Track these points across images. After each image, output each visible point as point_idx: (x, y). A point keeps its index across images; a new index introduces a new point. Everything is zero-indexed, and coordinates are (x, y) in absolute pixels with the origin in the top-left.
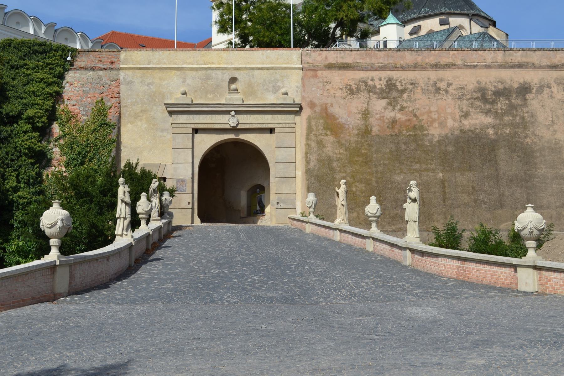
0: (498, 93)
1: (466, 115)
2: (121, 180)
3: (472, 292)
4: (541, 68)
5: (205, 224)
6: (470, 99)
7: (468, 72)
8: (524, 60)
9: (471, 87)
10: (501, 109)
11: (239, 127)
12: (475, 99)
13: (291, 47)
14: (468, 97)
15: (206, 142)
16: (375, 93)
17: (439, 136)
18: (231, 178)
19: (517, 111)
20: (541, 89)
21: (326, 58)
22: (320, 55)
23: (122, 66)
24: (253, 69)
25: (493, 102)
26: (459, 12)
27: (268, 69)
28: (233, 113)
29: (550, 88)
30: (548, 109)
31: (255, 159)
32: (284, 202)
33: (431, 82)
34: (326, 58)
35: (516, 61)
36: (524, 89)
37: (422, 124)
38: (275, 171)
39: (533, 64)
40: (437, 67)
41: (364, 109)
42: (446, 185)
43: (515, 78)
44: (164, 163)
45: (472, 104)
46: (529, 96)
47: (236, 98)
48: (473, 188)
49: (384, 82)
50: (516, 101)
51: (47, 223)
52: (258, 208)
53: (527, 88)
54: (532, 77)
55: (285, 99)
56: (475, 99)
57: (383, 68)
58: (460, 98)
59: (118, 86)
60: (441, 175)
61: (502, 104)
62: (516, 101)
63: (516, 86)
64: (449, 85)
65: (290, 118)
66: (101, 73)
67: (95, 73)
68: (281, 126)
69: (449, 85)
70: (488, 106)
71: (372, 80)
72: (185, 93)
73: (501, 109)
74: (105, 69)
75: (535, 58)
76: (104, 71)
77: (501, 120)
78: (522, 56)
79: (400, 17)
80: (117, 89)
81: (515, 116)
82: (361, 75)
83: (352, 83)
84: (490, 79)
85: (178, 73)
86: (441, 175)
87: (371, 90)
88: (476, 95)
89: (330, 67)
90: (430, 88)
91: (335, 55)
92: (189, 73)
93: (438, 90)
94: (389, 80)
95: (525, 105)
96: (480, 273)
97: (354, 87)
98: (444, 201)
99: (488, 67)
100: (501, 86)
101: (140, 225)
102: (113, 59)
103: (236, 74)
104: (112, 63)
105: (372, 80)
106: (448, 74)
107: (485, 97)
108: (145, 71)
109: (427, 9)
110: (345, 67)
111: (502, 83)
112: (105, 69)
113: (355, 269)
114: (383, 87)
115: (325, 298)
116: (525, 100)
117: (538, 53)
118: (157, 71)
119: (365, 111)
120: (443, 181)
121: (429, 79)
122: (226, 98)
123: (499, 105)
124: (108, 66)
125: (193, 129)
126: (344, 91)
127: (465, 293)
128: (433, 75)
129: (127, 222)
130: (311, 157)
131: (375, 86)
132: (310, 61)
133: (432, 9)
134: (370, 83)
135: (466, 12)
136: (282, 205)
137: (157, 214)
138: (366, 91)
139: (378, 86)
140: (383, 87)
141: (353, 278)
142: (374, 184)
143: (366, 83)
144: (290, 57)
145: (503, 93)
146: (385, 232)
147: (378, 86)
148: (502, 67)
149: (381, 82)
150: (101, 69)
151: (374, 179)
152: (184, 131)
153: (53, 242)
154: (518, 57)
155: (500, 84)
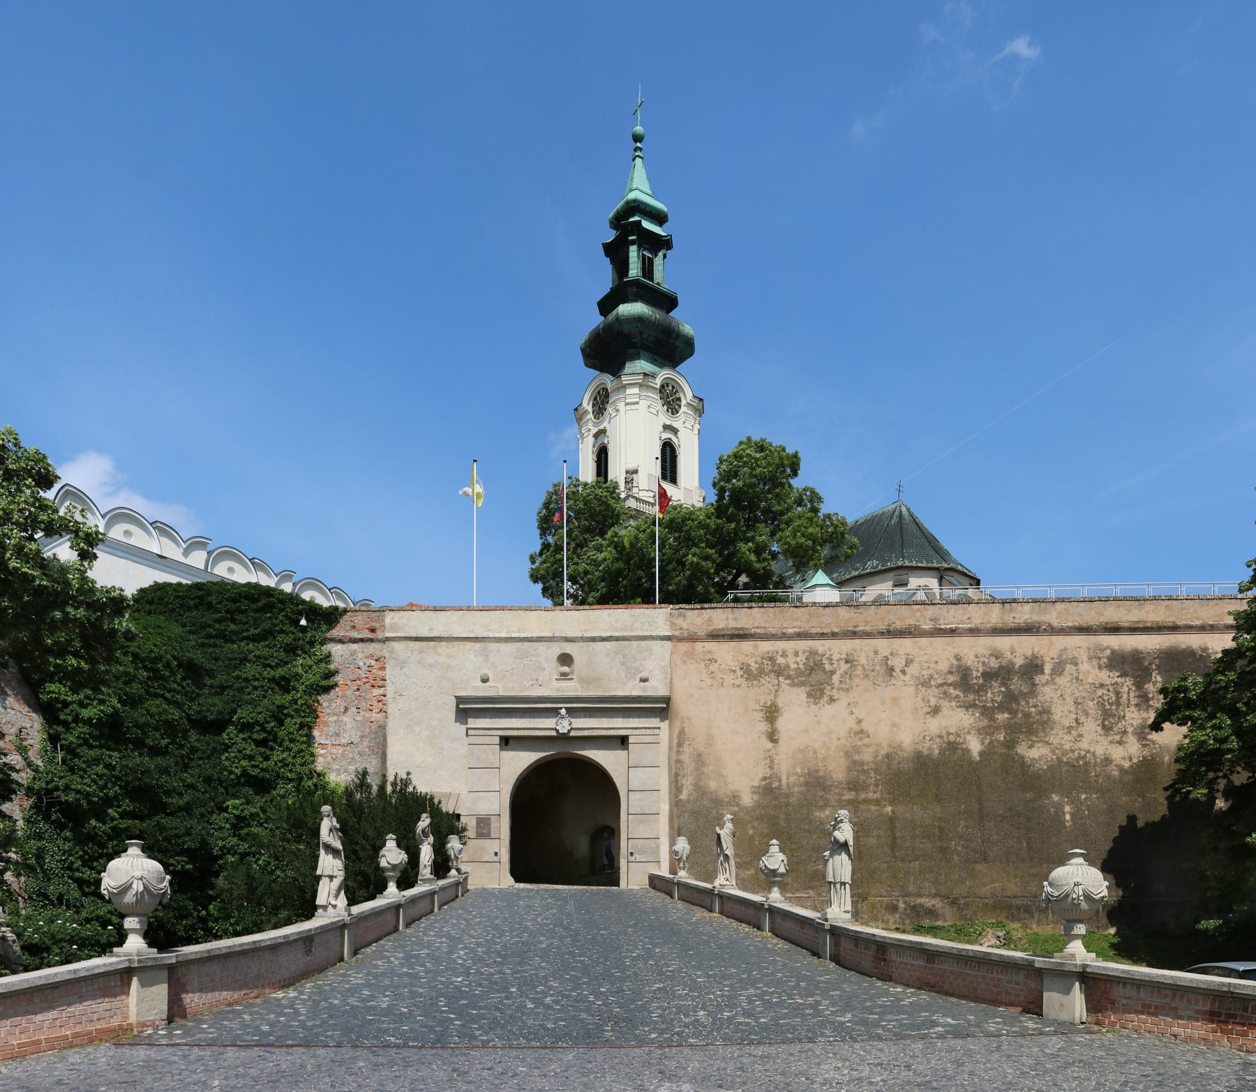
0: (988, 675)
1: (935, 711)
2: (326, 809)
3: (949, 1020)
4: (1062, 631)
5: (522, 885)
6: (942, 685)
7: (939, 642)
8: (1036, 618)
9: (944, 666)
10: (993, 701)
11: (573, 734)
12: (950, 685)
13: (654, 602)
14: (940, 681)
15: (524, 759)
16: (788, 677)
17: (890, 746)
18: (563, 816)
19: (1018, 704)
20: (1058, 670)
21: (710, 619)
22: (699, 616)
23: (388, 635)
24: (593, 639)
25: (981, 690)
26: (924, 565)
27: (617, 639)
28: (563, 712)
29: (1076, 664)
30: (1070, 700)
31: (602, 788)
32: (642, 852)
33: (879, 657)
34: (710, 619)
35: (1022, 621)
36: (1033, 667)
37: (849, 916)
38: (630, 804)
39: (1050, 625)
40: (890, 633)
41: (769, 703)
42: (898, 824)
43: (1018, 649)
44: (457, 791)
45: (945, 693)
46: (1039, 679)
47: (571, 689)
48: (941, 829)
49: (802, 658)
50: (1017, 685)
51: (113, 884)
52: (606, 862)
53: (1037, 666)
54: (1047, 648)
55: (644, 689)
56: (950, 685)
57: (801, 636)
58: (925, 684)
59: (383, 668)
60: (889, 809)
61: (994, 693)
62: (1017, 685)
63: (1019, 662)
64: (909, 662)
65: (653, 722)
66: (355, 646)
67: (345, 646)
68: (638, 732)
69: (909, 662)
70: (971, 697)
71: (784, 655)
72: (485, 680)
73: (993, 701)
74: (362, 640)
75: (1053, 616)
76: (361, 645)
77: (992, 719)
78: (1032, 612)
79: (835, 575)
80: (381, 673)
81: (1013, 712)
82: (766, 646)
83: (751, 662)
84: (974, 651)
85: (478, 645)
86: (889, 809)
87: (779, 672)
88: (951, 679)
89: (715, 636)
90: (878, 668)
91: (724, 616)
92: (493, 646)
93: (891, 670)
94: (813, 653)
95: (1033, 692)
96: (965, 980)
97: (754, 667)
98: (892, 849)
99: (974, 632)
100: (994, 663)
101: (385, 888)
102: (374, 624)
103: (568, 648)
104: (373, 630)
105: (784, 655)
106: (905, 645)
107: (964, 681)
108: (424, 644)
109: (875, 563)
110: (740, 635)
111: (997, 658)
112: (362, 640)
113: (733, 967)
114: (801, 666)
115: (662, 1032)
116: (1034, 685)
117: (1059, 606)
118: (444, 644)
119: (770, 707)
120: (892, 820)
121: (876, 653)
122: (552, 687)
123: (989, 695)
124: (366, 634)
125: (501, 737)
126: (739, 673)
127: (935, 1024)
128: (883, 645)
129: (337, 882)
130: (684, 781)
131: (787, 666)
132: (685, 626)
133: (884, 561)
134: (780, 660)
135: (935, 565)
136: (638, 857)
137: (428, 870)
138: (772, 675)
139: (793, 666)
140: (801, 666)
141: (726, 986)
142: (783, 823)
143: (772, 659)
144: (655, 618)
145: (1001, 674)
146: (789, 900)
147: (793, 666)
148: (997, 631)
149: (798, 659)
150: (355, 641)
151: (782, 816)
152: (487, 740)
153: (130, 923)
154: (1024, 614)
155: (993, 659)
